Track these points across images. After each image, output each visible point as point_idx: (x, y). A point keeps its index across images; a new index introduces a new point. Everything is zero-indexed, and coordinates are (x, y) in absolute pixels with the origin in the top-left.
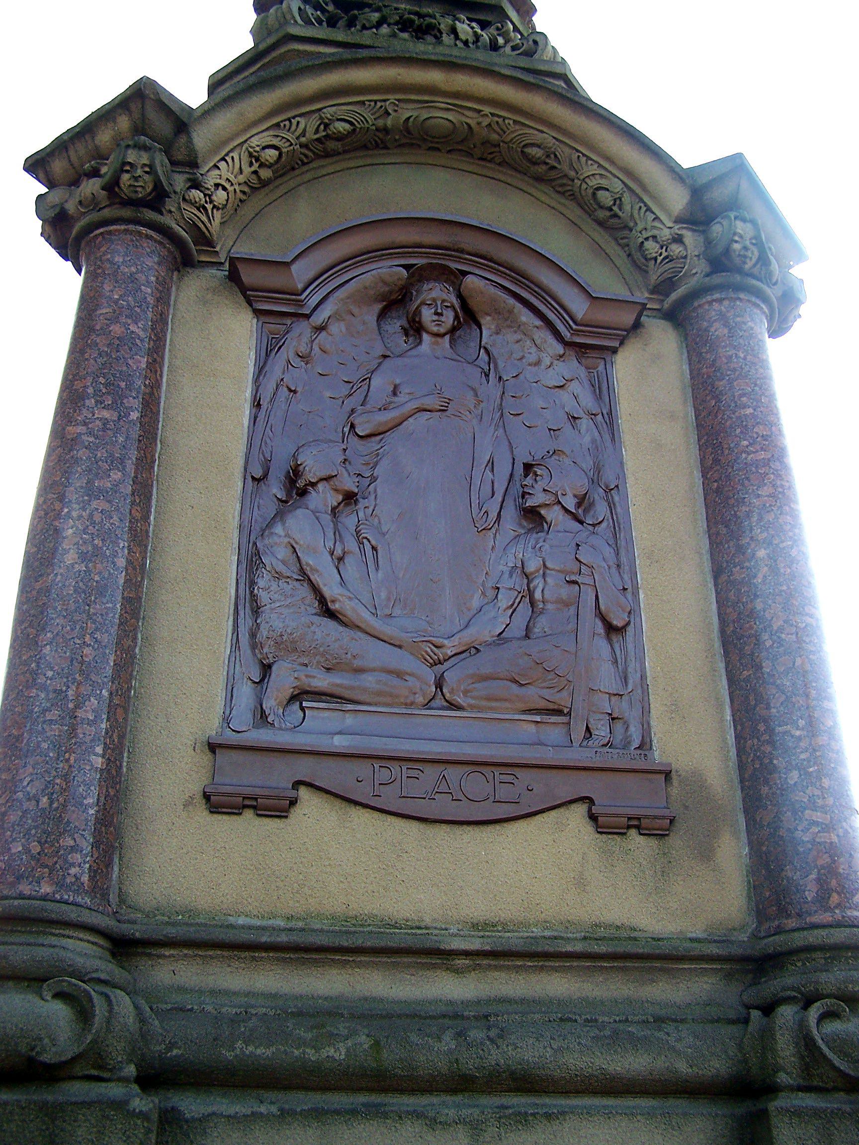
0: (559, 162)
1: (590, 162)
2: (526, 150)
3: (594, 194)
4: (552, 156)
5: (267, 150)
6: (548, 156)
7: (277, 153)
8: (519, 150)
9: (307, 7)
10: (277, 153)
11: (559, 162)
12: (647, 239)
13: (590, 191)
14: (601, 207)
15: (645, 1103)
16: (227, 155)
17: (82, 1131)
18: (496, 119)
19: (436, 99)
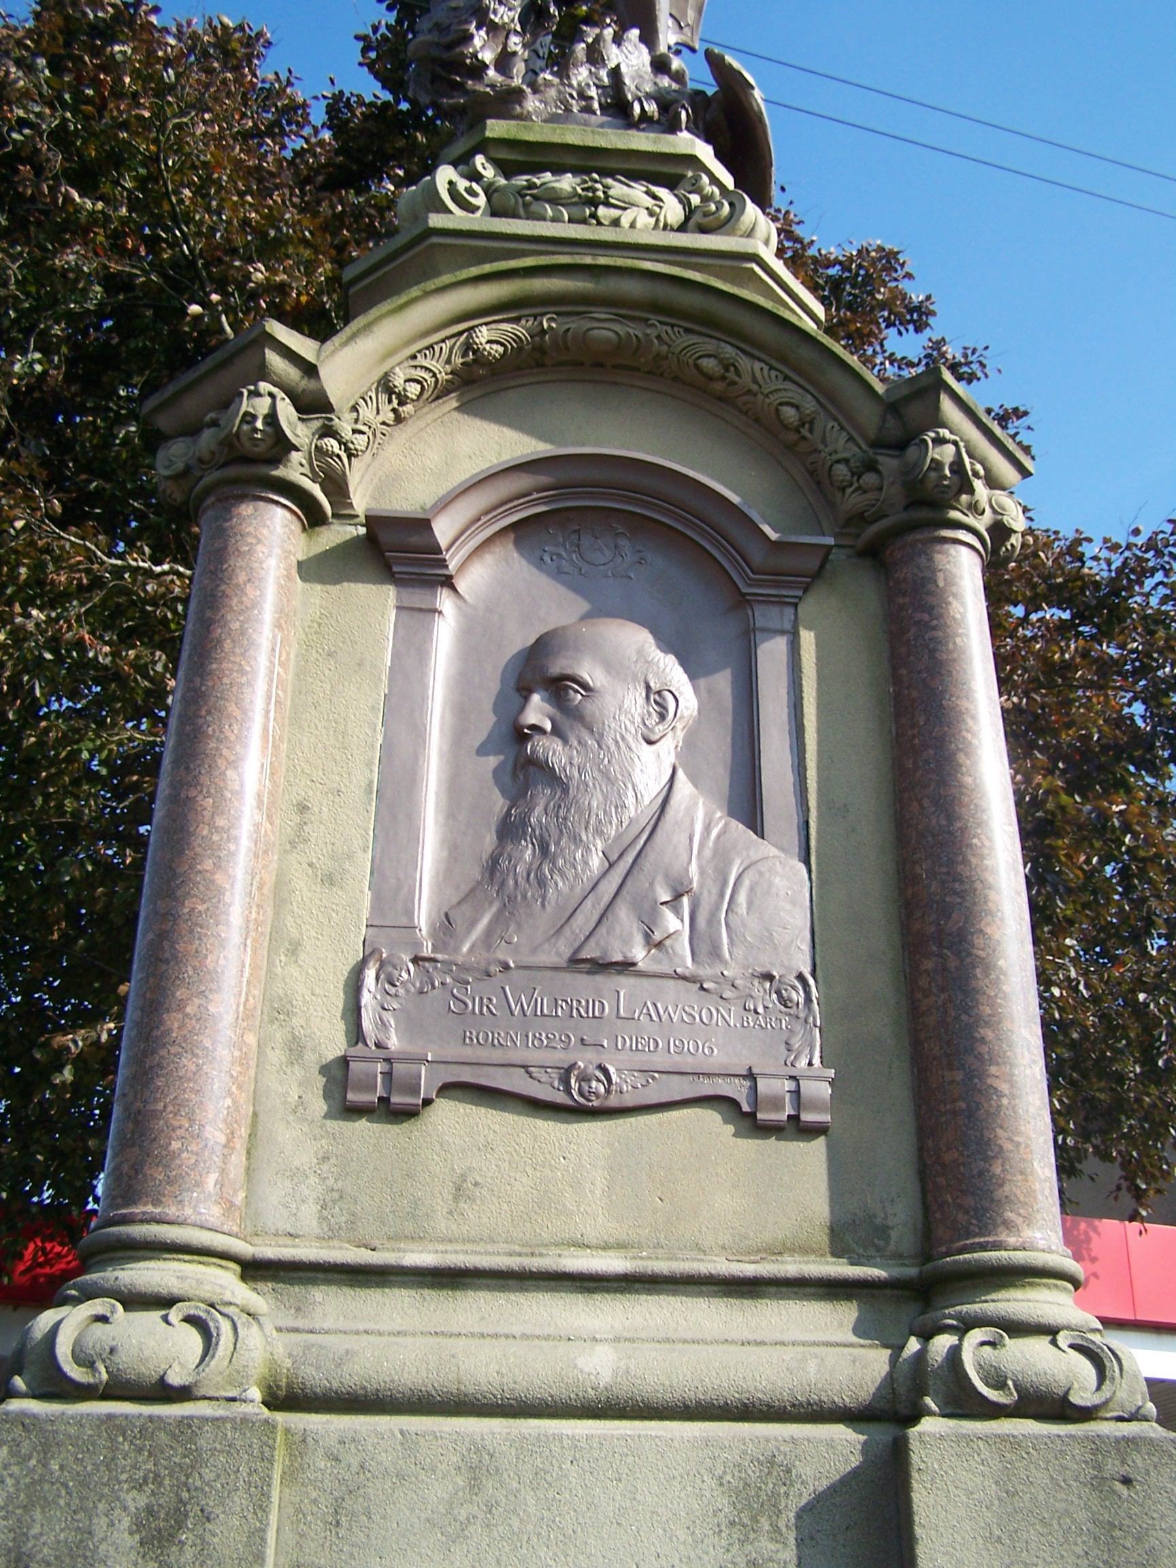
0: (740, 377)
1: (773, 373)
2: (700, 361)
3: (777, 410)
4: (732, 369)
5: (412, 384)
6: (727, 370)
7: (419, 387)
8: (691, 361)
9: (86, 200)
10: (419, 387)
11: (740, 377)
12: (838, 462)
13: (772, 409)
14: (786, 427)
15: (812, 1290)
16: (437, 343)
17: (267, 1532)
18: (665, 328)
19: (592, 309)
